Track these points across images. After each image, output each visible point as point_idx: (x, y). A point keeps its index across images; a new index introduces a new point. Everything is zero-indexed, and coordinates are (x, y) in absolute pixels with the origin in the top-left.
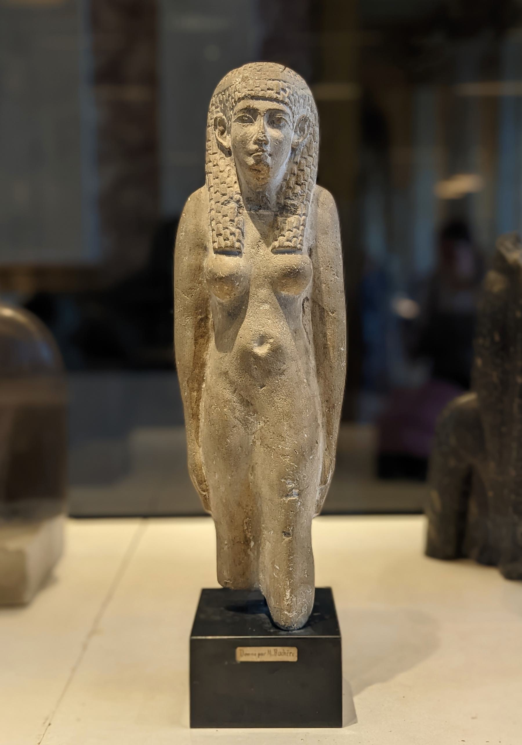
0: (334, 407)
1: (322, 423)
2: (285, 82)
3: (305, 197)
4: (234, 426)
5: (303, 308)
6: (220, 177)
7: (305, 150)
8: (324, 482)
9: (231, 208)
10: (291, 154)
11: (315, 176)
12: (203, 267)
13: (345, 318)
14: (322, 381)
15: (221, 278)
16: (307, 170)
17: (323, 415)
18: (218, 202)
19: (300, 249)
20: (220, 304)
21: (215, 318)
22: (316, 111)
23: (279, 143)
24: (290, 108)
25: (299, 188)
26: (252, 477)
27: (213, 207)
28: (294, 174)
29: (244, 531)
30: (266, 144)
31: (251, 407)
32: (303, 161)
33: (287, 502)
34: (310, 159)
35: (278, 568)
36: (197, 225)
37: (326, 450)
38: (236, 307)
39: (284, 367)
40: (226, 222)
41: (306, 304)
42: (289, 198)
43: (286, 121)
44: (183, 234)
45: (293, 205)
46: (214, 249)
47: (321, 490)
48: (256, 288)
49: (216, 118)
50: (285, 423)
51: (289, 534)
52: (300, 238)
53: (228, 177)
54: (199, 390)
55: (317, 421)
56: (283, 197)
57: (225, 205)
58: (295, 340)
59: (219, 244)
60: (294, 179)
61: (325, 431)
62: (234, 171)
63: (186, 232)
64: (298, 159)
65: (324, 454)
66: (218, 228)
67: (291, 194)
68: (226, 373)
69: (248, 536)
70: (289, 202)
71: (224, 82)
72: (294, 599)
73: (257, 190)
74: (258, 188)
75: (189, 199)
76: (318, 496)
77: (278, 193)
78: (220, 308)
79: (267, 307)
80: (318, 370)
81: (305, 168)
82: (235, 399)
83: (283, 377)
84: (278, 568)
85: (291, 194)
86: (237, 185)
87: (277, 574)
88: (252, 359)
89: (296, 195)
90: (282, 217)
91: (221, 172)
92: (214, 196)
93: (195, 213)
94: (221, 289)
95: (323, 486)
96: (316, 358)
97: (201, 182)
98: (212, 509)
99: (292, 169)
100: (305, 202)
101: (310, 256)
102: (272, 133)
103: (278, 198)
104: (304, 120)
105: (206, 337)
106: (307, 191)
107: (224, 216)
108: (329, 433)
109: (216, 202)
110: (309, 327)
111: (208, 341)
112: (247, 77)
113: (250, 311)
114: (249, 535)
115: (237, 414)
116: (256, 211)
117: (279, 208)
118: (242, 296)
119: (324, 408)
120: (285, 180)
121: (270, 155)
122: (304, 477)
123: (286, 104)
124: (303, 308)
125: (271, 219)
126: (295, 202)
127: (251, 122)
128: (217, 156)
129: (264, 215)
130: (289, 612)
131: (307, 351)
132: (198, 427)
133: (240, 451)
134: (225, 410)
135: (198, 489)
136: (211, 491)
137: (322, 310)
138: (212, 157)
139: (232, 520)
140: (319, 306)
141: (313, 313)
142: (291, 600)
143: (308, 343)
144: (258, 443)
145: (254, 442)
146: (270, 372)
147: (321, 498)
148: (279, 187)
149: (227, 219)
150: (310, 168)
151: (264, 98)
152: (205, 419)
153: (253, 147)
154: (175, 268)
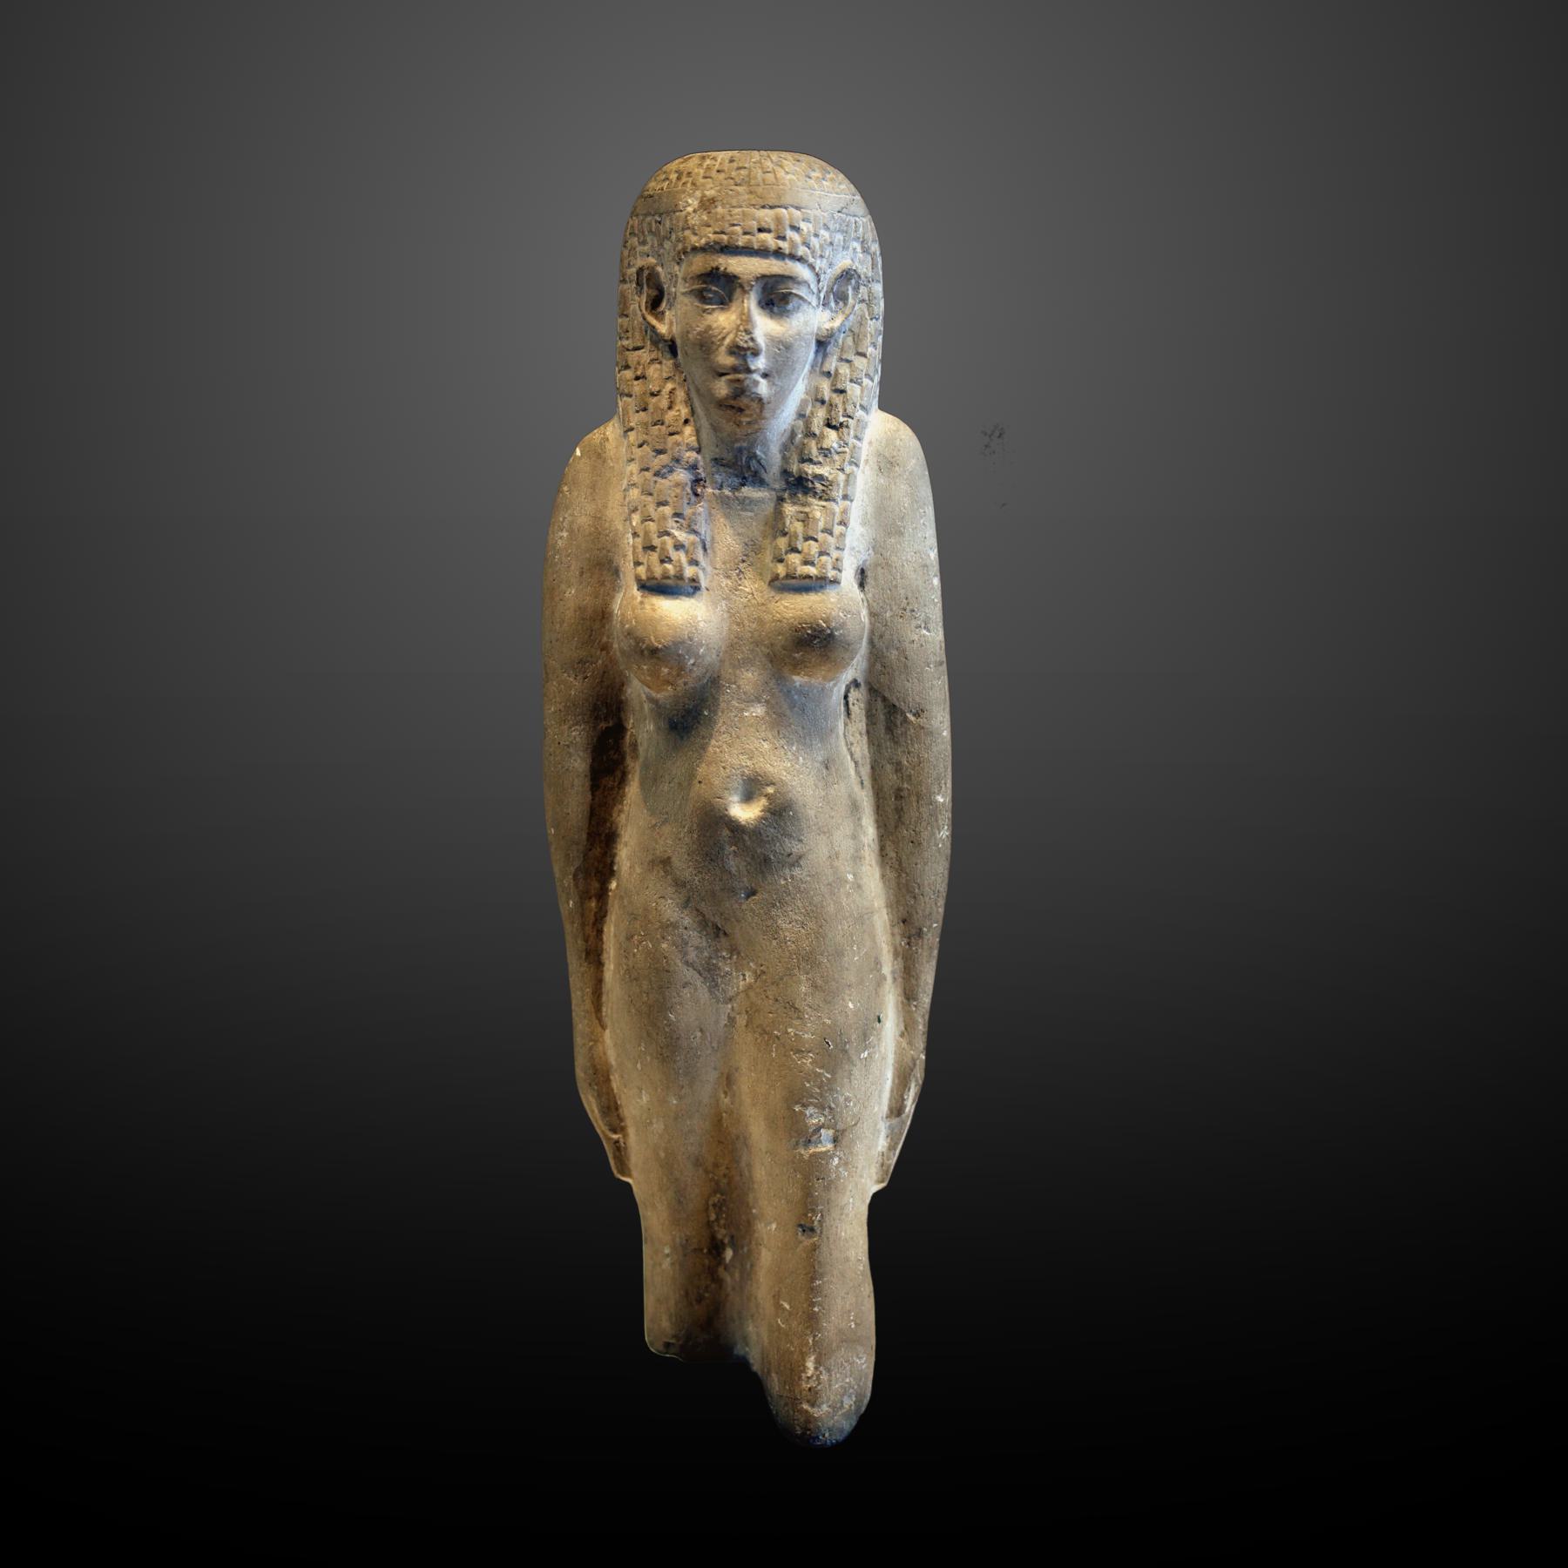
0: (920, 934)
1: (893, 972)
2: (798, 208)
3: (848, 457)
4: (685, 985)
5: (847, 704)
6: (651, 408)
7: (850, 341)
8: (896, 1111)
9: (677, 485)
10: (817, 352)
11: (872, 385)
12: (611, 614)
13: (947, 724)
14: (891, 875)
15: (654, 652)
16: (854, 391)
17: (896, 954)
18: (647, 470)
19: (835, 582)
20: (651, 700)
21: (643, 731)
23: (783, 349)
24: (812, 267)
25: (832, 435)
26: (727, 1100)
27: (635, 478)
28: (823, 402)
29: (709, 1224)
30: (756, 353)
31: (723, 940)
32: (845, 370)
33: (806, 1157)
34: (860, 363)
35: (787, 1306)
36: (598, 518)
37: (902, 1035)
38: (689, 712)
39: (796, 848)
40: (664, 518)
41: (853, 695)
42: (810, 461)
43: (801, 298)
44: (565, 534)
45: (820, 478)
46: (638, 580)
47: (891, 1128)
48: (734, 667)
49: (641, 270)
50: (803, 978)
51: (812, 1230)
52: (835, 554)
53: (670, 408)
54: (602, 895)
55: (879, 970)
56: (795, 458)
57: (664, 477)
58: (827, 785)
59: (649, 569)
60: (821, 414)
61: (899, 990)
62: (680, 395)
63: (571, 531)
64: (832, 364)
65: (898, 1045)
66: (647, 533)
67: (814, 451)
68: (666, 862)
69: (719, 1236)
70: (810, 469)
72: (824, 1377)
73: (737, 445)
74: (737, 440)
76: (882, 1143)
77: (785, 448)
78: (652, 710)
79: (759, 710)
80: (882, 849)
81: (849, 386)
82: (687, 921)
83: (797, 872)
84: (787, 1306)
85: (814, 451)
86: (688, 430)
87: (786, 1321)
88: (726, 832)
89: (825, 452)
90: (794, 504)
91: (653, 394)
92: (638, 452)
93: (593, 487)
94: (655, 673)
95: (895, 1121)
96: (877, 821)
98: (634, 1173)
99: (817, 389)
100: (848, 469)
101: (862, 585)
102: (764, 327)
103: (785, 458)
105: (618, 774)
106: (852, 441)
107: (660, 504)
108: (909, 996)
109: (643, 470)
110: (861, 748)
111: (623, 781)
112: (713, 201)
113: (721, 722)
114: (721, 1233)
115: (692, 955)
116: (735, 489)
117: (788, 483)
118: (703, 687)
119: (898, 938)
120: (801, 415)
121: (765, 376)
122: (847, 1099)
123: (800, 259)
124: (847, 704)
125: (769, 508)
126: (824, 471)
127: (724, 302)
129: (751, 501)
130: (813, 1405)
131: (855, 807)
132: (599, 981)
133: (698, 1040)
134: (664, 946)
135: (600, 1126)
136: (631, 1131)
137: (892, 710)
139: (687, 1294)
140: (884, 699)
141: (870, 716)
142: (818, 1378)
143: (857, 788)
144: (741, 1021)
145: (732, 1020)
146: (766, 860)
147: (891, 1148)
148: (787, 435)
149: (667, 510)
150: (860, 384)
151: (748, 251)
152: (618, 965)
153: (726, 360)
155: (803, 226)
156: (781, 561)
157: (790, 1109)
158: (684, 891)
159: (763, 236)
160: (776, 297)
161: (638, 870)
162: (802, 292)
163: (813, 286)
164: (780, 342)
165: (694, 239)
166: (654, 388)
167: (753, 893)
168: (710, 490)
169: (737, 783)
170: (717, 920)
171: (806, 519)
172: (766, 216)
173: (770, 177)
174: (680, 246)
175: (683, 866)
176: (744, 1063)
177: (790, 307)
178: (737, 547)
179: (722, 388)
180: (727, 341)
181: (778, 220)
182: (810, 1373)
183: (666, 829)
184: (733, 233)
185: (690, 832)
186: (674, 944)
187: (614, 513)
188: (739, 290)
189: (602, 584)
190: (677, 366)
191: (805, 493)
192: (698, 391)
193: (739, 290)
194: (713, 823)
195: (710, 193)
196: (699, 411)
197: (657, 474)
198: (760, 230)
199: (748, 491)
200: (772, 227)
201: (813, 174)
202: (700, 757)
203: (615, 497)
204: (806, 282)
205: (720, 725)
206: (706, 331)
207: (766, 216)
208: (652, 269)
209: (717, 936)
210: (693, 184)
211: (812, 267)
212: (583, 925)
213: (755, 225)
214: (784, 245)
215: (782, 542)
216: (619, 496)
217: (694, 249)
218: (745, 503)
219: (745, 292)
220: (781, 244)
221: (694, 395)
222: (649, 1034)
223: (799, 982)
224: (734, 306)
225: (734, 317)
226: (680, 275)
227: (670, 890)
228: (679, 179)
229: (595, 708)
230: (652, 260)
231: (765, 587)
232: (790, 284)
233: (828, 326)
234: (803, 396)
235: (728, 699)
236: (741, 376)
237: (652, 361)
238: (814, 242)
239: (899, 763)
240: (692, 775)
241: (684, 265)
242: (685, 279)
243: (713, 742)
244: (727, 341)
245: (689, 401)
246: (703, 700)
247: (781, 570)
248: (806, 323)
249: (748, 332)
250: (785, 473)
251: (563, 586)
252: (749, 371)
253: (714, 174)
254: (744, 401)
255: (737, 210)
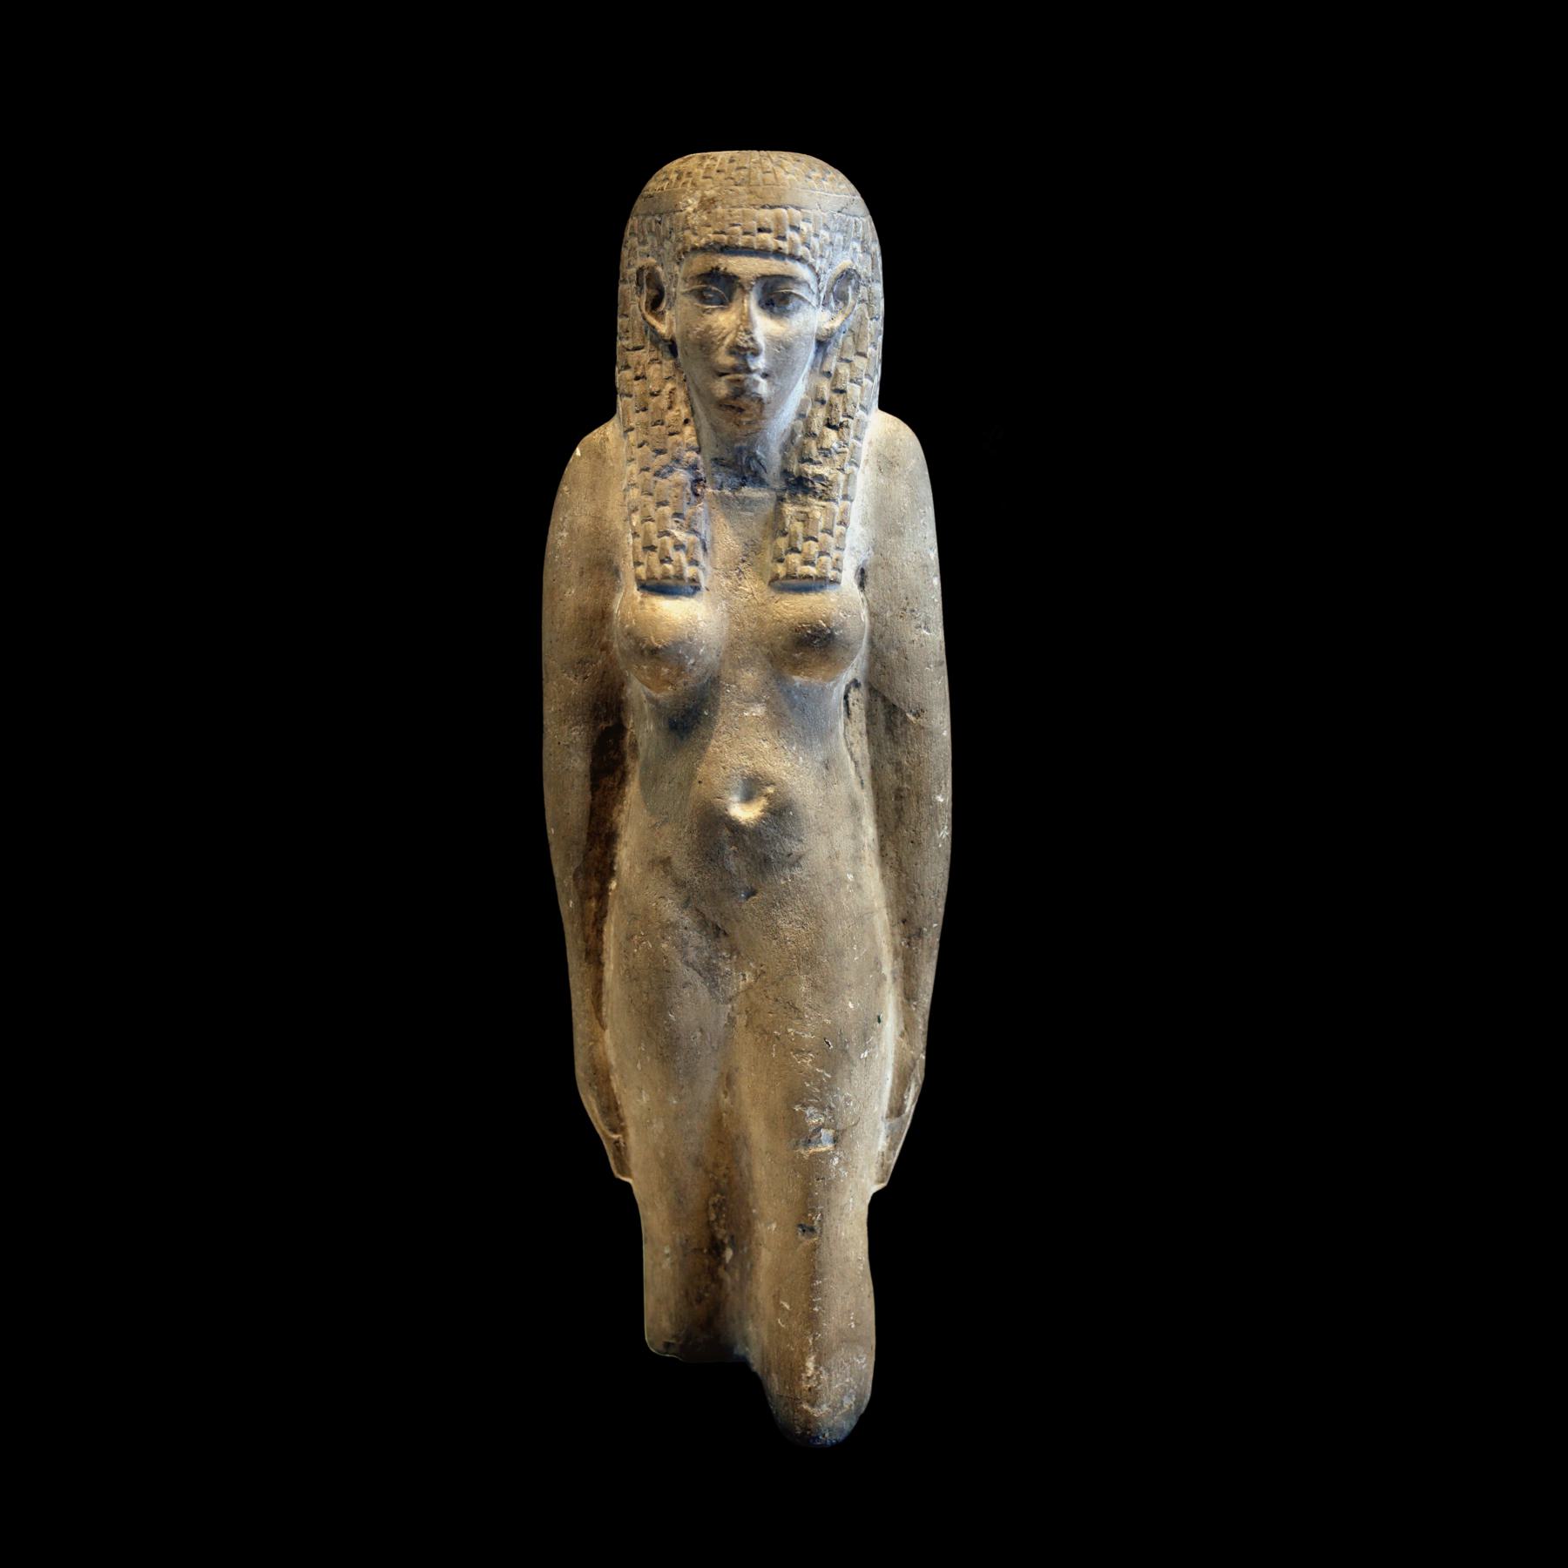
0: (920, 934)
1: (893, 972)
2: (798, 208)
3: (848, 457)
4: (685, 985)
5: (847, 704)
6: (651, 408)
7: (850, 341)
8: (896, 1111)
9: (677, 485)
10: (817, 352)
12: (611, 614)
14: (891, 875)
15: (654, 652)
16: (854, 391)
17: (896, 954)
18: (647, 470)
19: (835, 582)
20: (651, 700)
21: (643, 731)
22: (876, 247)
23: (783, 349)
24: (812, 267)
25: (832, 435)
26: (727, 1100)
27: (635, 478)
28: (823, 402)
29: (709, 1224)
30: (756, 353)
31: (723, 940)
32: (845, 370)
33: (806, 1157)
34: (860, 363)
35: (787, 1306)
36: (598, 518)
37: (902, 1035)
38: (689, 712)
39: (796, 848)
40: (664, 518)
41: (853, 695)
42: (810, 461)
43: (801, 298)
44: (565, 534)
45: (820, 478)
46: (638, 580)
47: (891, 1128)
48: (734, 667)
49: (641, 270)
50: (803, 978)
51: (812, 1230)
52: (835, 554)
53: (670, 408)
54: (602, 895)
55: (879, 970)
56: (795, 458)
57: (664, 477)
58: (827, 785)
59: (649, 569)
60: (821, 414)
61: (899, 990)
62: (680, 395)
63: (571, 531)
64: (832, 364)
65: (898, 1045)
66: (647, 533)
67: (814, 451)
68: (666, 862)
69: (719, 1236)
70: (810, 469)
71: (653, 185)
72: (824, 1377)
73: (737, 445)
74: (737, 440)
75: (578, 452)
76: (882, 1143)
77: (785, 448)
78: (652, 710)
79: (759, 710)
80: (882, 849)
81: (849, 386)
82: (687, 921)
83: (797, 872)
84: (787, 1306)
85: (814, 451)
86: (688, 430)
87: (786, 1321)
88: (726, 832)
89: (825, 452)
90: (794, 504)
91: (653, 394)
92: (638, 452)
93: (593, 487)
94: (655, 673)
95: (895, 1121)
96: (877, 821)
97: (605, 411)
98: (634, 1173)
99: (817, 389)
100: (848, 469)
101: (862, 585)
102: (764, 327)
103: (785, 458)
104: (847, 275)
105: (618, 774)
106: (852, 441)
107: (660, 504)
108: (909, 996)
109: (643, 470)
110: (861, 748)
111: (623, 781)
112: (713, 201)
113: (721, 722)
114: (721, 1233)
115: (692, 955)
116: (735, 489)
117: (788, 483)
118: (703, 687)
119: (898, 938)
120: (801, 415)
121: (765, 376)
122: (847, 1099)
123: (800, 259)
124: (847, 704)
125: (769, 508)
126: (824, 471)
127: (724, 302)
128: (645, 355)
129: (751, 501)
130: (813, 1405)
131: (855, 807)
132: (599, 981)
133: (698, 1040)
134: (664, 946)
136: (631, 1131)
137: (892, 710)
138: (633, 357)
139: (687, 1294)
140: (884, 699)
141: (870, 716)
142: (818, 1378)
143: (857, 788)
144: (741, 1021)
145: (732, 1020)
146: (766, 860)
147: (891, 1148)
148: (787, 435)
149: (667, 510)
150: (860, 384)
151: (748, 251)
152: (618, 965)
153: (726, 360)
154: (546, 613)
155: (803, 226)
156: (781, 561)
157: (790, 1109)
158: (684, 891)
159: (763, 236)
160: (776, 297)
161: (638, 870)
162: (802, 292)
163: (813, 286)
164: (780, 342)
165: (694, 239)
166: (654, 388)
167: (753, 893)
168: (710, 490)
169: (737, 783)
170: (717, 920)
171: (806, 519)
172: (766, 216)
173: (770, 177)
174: (680, 246)
175: (683, 866)
176: (744, 1063)
177: (790, 307)
178: (737, 547)
179: (722, 388)
180: (727, 341)
181: (778, 220)
182: (810, 1373)
183: (666, 829)
184: (733, 233)
185: (690, 832)
186: (674, 944)
187: (614, 513)
188: (739, 290)
189: (602, 584)
190: (677, 366)
191: (805, 493)
192: (698, 391)
193: (739, 290)
194: (713, 823)
195: (710, 193)
196: (699, 411)
197: (657, 474)
198: (760, 230)
199: (748, 491)
200: (772, 227)
201: (813, 174)
202: (700, 757)
203: (615, 497)
204: (806, 282)
205: (720, 725)
206: (706, 331)
207: (766, 216)
208: (652, 269)
209: (717, 936)
210: (693, 184)
211: (812, 267)
212: (583, 925)
213: (755, 225)
214: (784, 245)
215: (782, 542)
216: (619, 496)
217: (694, 249)
218: (745, 503)
219: (745, 292)
220: (781, 244)
221: (694, 395)
222: (649, 1034)
223: (799, 982)
224: (734, 306)
225: (734, 317)
226: (680, 275)
227: (670, 890)
228: (679, 179)
229: (595, 708)
230: (652, 260)
231: (765, 587)
232: (790, 284)
233: (828, 326)
234: (803, 396)
235: (728, 699)
236: (741, 376)
237: (652, 361)
238: (814, 242)
239: (899, 763)
240: (692, 775)
241: (684, 265)
242: (685, 279)
243: (713, 742)
244: (727, 341)
245: (689, 401)
246: (703, 700)
247: (781, 570)
248: (806, 323)
249: (748, 332)
250: (785, 473)
251: (563, 586)
252: (749, 371)
253: (714, 174)
254: (744, 401)
255: (737, 210)
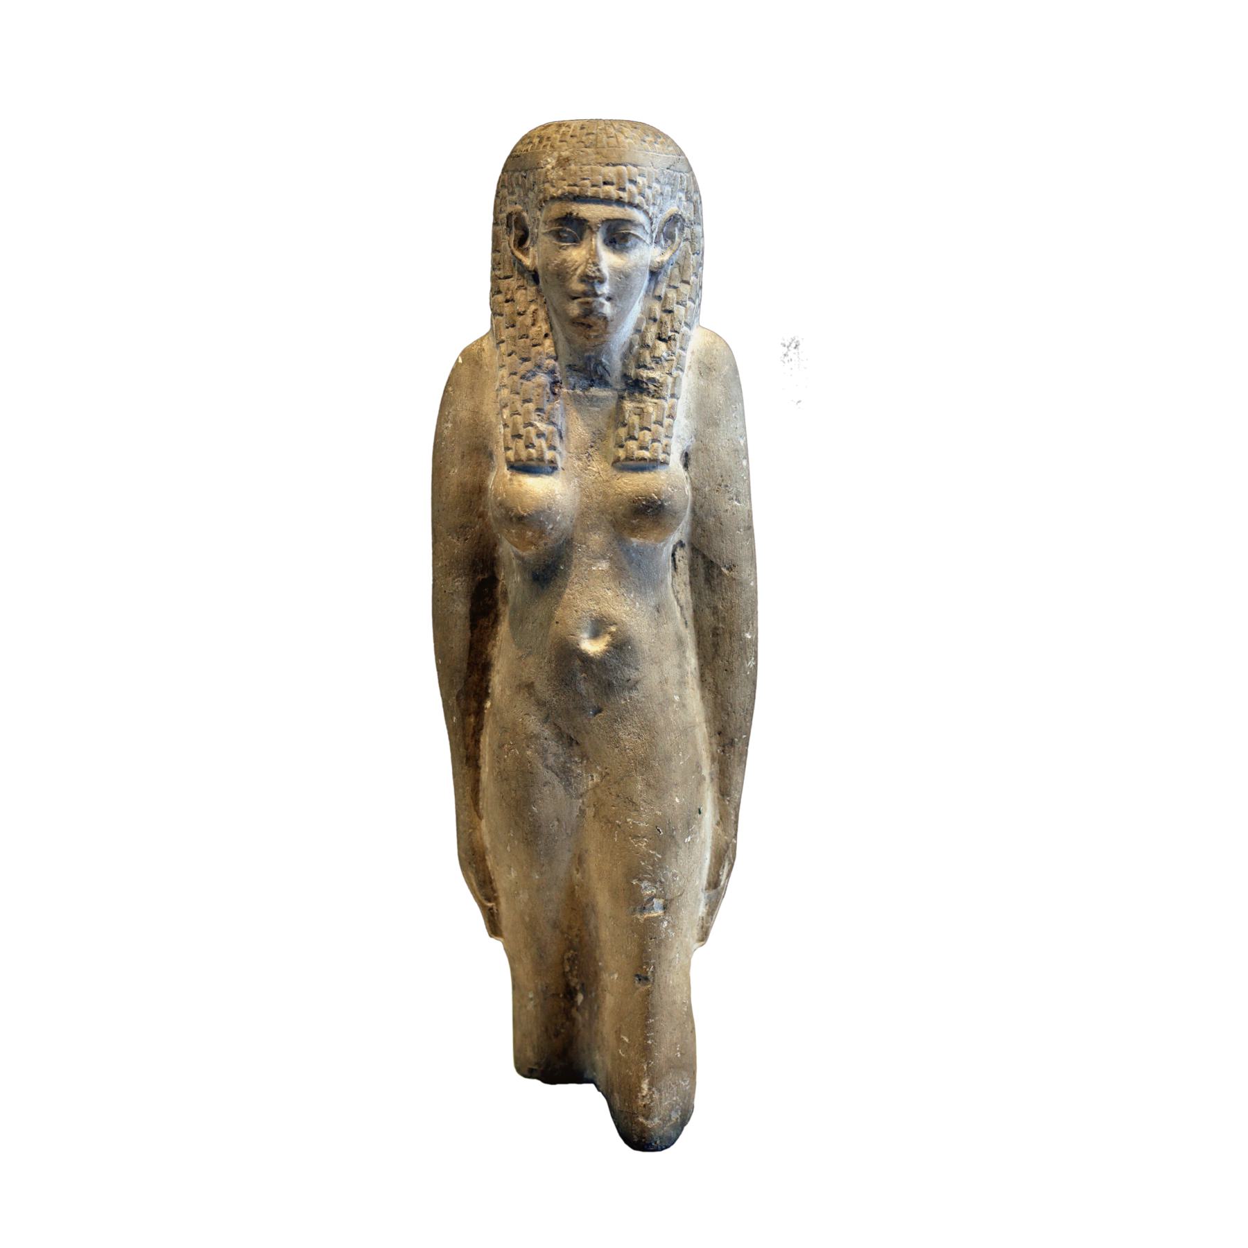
1: (711, 774)
2: (635, 166)
3: (675, 364)
4: (546, 784)
5: (674, 560)
6: (518, 325)
7: (676, 271)
9: (539, 386)
10: (650, 280)
12: (486, 489)
14: (709, 696)
15: (521, 519)
17: (713, 759)
18: (515, 374)
19: (665, 463)
20: (518, 557)
21: (512, 582)
23: (623, 278)
24: (646, 213)
25: (662, 346)
26: (578, 876)
27: (505, 381)
28: (655, 320)
29: (564, 974)
30: (602, 281)
31: (576, 748)
32: (672, 294)
33: (642, 921)
35: (626, 1040)
36: (476, 412)
37: (718, 824)
38: (548, 566)
39: (634, 675)
40: (528, 412)
41: (679, 553)
42: (645, 367)
43: (637, 237)
44: (450, 425)
45: (653, 380)
46: (508, 461)
48: (584, 531)
49: (510, 215)
50: (639, 778)
51: (646, 979)
52: (664, 441)
53: (533, 325)
54: (479, 712)
55: (700, 772)
56: (633, 364)
57: (528, 379)
58: (658, 625)
59: (516, 453)
60: (654, 329)
61: (716, 788)
62: (542, 314)
63: (454, 423)
64: (662, 290)
65: (715, 831)
66: (515, 424)
67: (648, 359)
68: (530, 686)
69: (573, 984)
70: (645, 374)
72: (656, 1096)
73: (587, 354)
74: (587, 351)
77: (625, 356)
78: (519, 565)
79: (604, 565)
80: (702, 675)
81: (676, 308)
82: (547, 733)
83: (634, 694)
84: (626, 1040)
85: (648, 359)
86: (548, 342)
87: (625, 1051)
88: (578, 662)
89: (657, 360)
90: (632, 401)
91: (519, 314)
92: (508, 360)
93: (472, 388)
94: (521, 536)
96: (698, 654)
99: (650, 310)
100: (675, 373)
101: (686, 466)
102: (608, 260)
103: (624, 365)
105: (492, 616)
106: (678, 351)
107: (526, 401)
109: (511, 374)
110: (686, 596)
111: (496, 621)
112: (567, 160)
113: (574, 574)
114: (574, 982)
115: (551, 760)
116: (585, 389)
117: (627, 384)
118: (560, 547)
119: (715, 747)
120: (637, 331)
121: (609, 299)
122: (674, 875)
123: (637, 207)
124: (674, 560)
125: (612, 404)
126: (656, 375)
127: (576, 241)
129: (598, 399)
130: (647, 1119)
131: (680, 642)
133: (556, 828)
134: (529, 753)
136: (502, 900)
137: (710, 565)
139: (547, 1030)
140: (704, 557)
141: (693, 570)
142: (651, 1097)
143: (682, 627)
144: (590, 812)
145: (582, 812)
146: (610, 685)
148: (626, 346)
149: (531, 406)
150: (684, 306)
151: (595, 200)
152: (492, 768)
153: (578, 287)
155: (639, 180)
156: (622, 446)
157: (629, 882)
158: (545, 709)
159: (607, 188)
160: (618, 236)
161: (508, 693)
162: (638, 232)
163: (647, 228)
164: (621, 272)
165: (552, 190)
166: (520, 308)
167: (599, 711)
168: (565, 390)
169: (587, 623)
170: (571, 732)
171: (641, 413)
172: (610, 172)
173: (613, 141)
174: (541, 196)
175: (543, 689)
176: (592, 846)
177: (629, 244)
178: (587, 436)
179: (574, 309)
180: (579, 272)
181: (620, 175)
182: (645, 1093)
183: (530, 660)
184: (583, 185)
185: (549, 662)
186: (536, 751)
187: (489, 409)
188: (588, 231)
189: (479, 464)
190: (539, 291)
191: (641, 393)
192: (555, 311)
193: (588, 231)
194: (568, 655)
195: (565, 154)
196: (557, 327)
197: (523, 377)
198: (605, 183)
199: (595, 391)
200: (615, 181)
202: (557, 603)
203: (490, 395)
204: (641, 225)
205: (573, 577)
206: (562, 264)
207: (610, 172)
208: (519, 214)
209: (571, 745)
210: (552, 146)
211: (646, 213)
213: (601, 179)
214: (624, 195)
215: (623, 432)
216: (493, 395)
217: (553, 198)
218: (593, 400)
219: (593, 232)
220: (622, 194)
221: (552, 314)
222: (516, 823)
223: (636, 782)
224: (585, 244)
225: (584, 252)
226: (541, 219)
227: (534, 708)
228: (540, 142)
229: (474, 564)
230: (519, 207)
231: (609, 467)
232: (629, 226)
233: (659, 259)
234: (639, 315)
235: (579, 556)
236: (590, 299)
237: (519, 287)
238: (648, 192)
239: (715, 608)
240: (550, 617)
241: (544, 211)
242: (545, 222)
243: (568, 591)
244: (579, 272)
245: (548, 319)
246: (560, 557)
247: (621, 453)
248: (642, 257)
249: (595, 264)
250: (625, 376)
251: (448, 467)
252: (596, 295)
253: (568, 138)
254: (592, 319)
255: (586, 167)
